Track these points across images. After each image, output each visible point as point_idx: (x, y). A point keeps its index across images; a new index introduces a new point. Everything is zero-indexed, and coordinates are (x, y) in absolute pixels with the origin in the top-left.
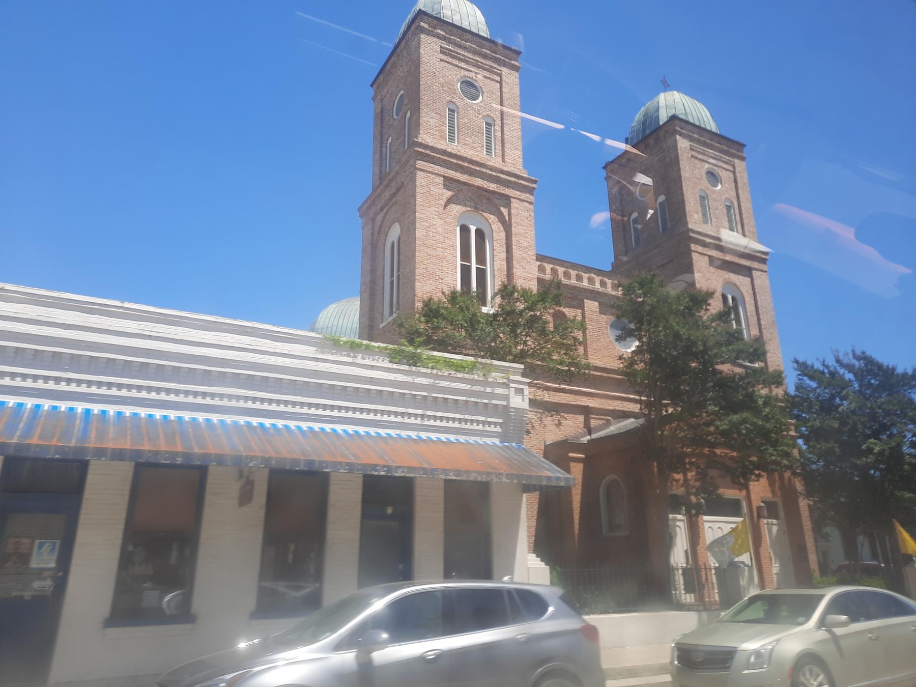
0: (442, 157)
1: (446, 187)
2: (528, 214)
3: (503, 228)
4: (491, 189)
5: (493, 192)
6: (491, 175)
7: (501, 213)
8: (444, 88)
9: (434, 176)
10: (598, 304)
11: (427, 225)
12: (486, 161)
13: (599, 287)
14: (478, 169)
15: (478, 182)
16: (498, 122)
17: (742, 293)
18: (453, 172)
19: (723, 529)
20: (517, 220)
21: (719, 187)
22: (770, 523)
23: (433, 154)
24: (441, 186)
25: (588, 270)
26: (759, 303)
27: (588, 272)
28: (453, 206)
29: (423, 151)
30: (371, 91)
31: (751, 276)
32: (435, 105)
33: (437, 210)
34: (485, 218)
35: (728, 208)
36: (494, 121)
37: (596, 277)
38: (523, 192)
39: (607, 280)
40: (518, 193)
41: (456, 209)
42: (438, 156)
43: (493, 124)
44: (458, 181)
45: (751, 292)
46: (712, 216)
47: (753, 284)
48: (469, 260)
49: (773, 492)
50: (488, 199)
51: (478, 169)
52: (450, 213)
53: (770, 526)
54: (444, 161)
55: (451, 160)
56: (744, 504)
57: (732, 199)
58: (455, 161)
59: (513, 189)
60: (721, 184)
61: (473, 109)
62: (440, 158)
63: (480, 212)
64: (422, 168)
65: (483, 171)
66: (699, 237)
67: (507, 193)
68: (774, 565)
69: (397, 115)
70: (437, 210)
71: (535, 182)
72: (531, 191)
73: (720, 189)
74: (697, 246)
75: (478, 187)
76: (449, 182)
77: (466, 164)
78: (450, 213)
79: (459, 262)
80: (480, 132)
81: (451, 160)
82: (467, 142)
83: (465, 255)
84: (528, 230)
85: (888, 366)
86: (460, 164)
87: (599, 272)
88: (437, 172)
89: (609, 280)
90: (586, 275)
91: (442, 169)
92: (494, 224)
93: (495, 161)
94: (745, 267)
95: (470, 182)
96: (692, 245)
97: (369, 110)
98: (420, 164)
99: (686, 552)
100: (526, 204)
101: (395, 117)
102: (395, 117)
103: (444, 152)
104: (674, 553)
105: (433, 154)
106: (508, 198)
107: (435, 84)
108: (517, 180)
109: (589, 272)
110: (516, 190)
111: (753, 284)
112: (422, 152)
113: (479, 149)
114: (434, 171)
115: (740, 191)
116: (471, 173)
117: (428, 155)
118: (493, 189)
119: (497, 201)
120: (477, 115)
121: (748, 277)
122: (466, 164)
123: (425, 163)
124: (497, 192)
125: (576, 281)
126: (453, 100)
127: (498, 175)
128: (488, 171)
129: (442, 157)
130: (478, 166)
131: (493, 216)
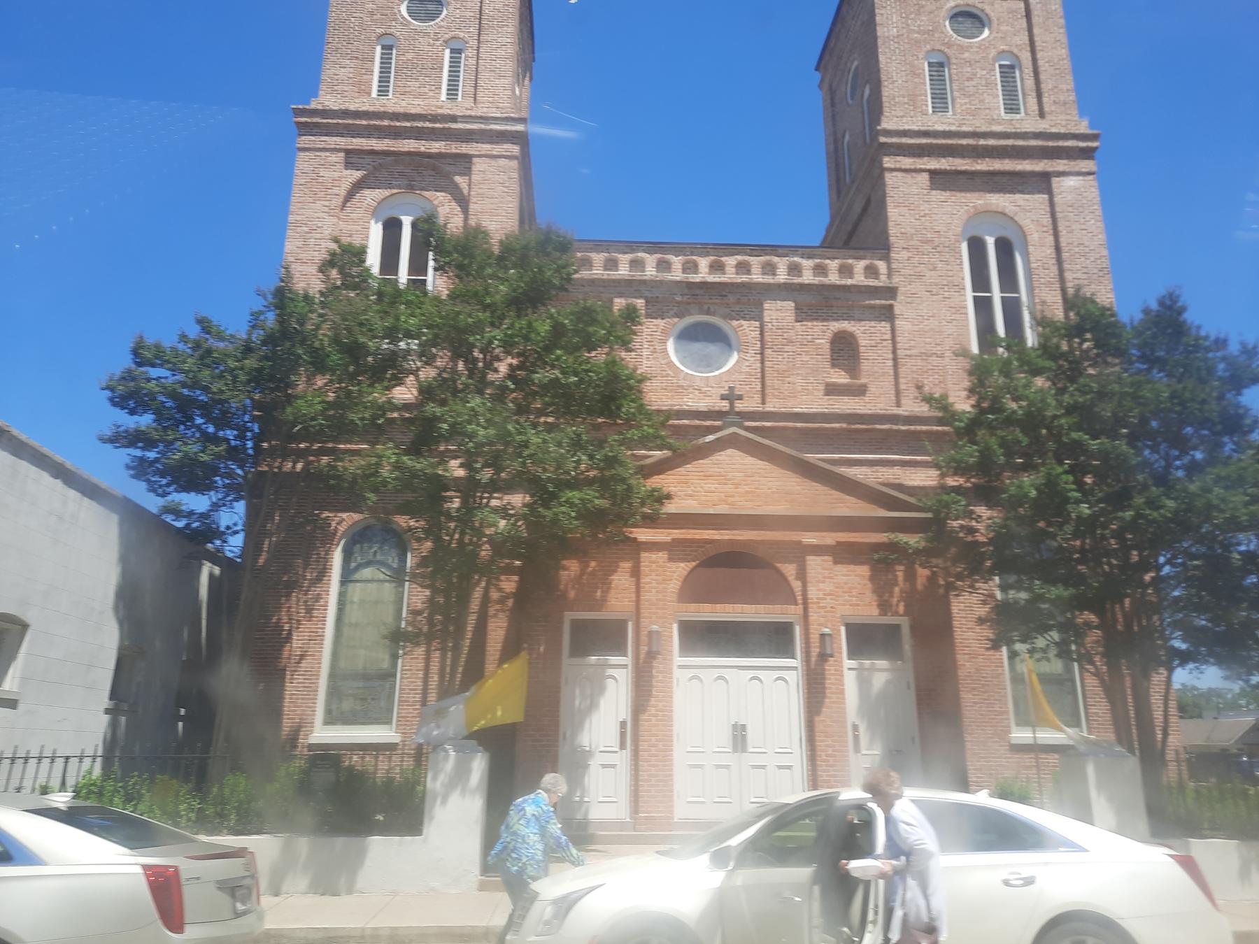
0: (340, 121)
1: (348, 165)
2: (505, 177)
3: (459, 209)
4: (432, 151)
5: (441, 156)
6: (433, 128)
7: (456, 186)
8: (375, 17)
9: (328, 154)
10: (793, 304)
11: (306, 229)
12: (433, 109)
13: (863, 279)
14: (408, 124)
15: (409, 145)
16: (1026, 56)
17: (1020, 227)
18: (363, 140)
19: (764, 682)
20: (480, 191)
21: (986, 33)
22: (867, 666)
23: (325, 121)
24: (341, 167)
25: (630, 246)
26: (1063, 242)
27: (633, 251)
28: (367, 192)
29: (308, 120)
30: (818, 75)
31: (1049, 191)
32: (350, 46)
33: (327, 203)
34: (1009, 216)
35: (1008, 72)
36: (1017, 57)
37: (648, 255)
38: (497, 143)
39: (674, 257)
40: (488, 146)
41: (371, 196)
42: (335, 121)
43: (946, 64)
44: (373, 152)
45: (1047, 220)
46: (956, 94)
47: (1052, 204)
48: (987, 288)
49: (884, 607)
50: (434, 169)
51: (408, 124)
52: (359, 205)
53: (866, 673)
54: (347, 126)
55: (358, 122)
56: (798, 630)
57: (1015, 51)
58: (364, 122)
59: (477, 143)
60: (990, 29)
61: (427, 34)
62: (338, 124)
63: (418, 192)
64: (306, 146)
65: (417, 127)
66: (1061, 143)
67: (465, 152)
68: (864, 752)
69: (852, 99)
70: (327, 203)
71: (1094, 137)
72: (1087, 154)
73: (988, 37)
74: (899, 158)
75: (409, 154)
76: (352, 158)
77: (386, 123)
78: (359, 205)
79: (969, 294)
80: (435, 66)
81: (358, 122)
82: (408, 89)
83: (981, 281)
84: (501, 202)
85: (1146, 311)
86: (375, 125)
87: (807, 252)
88: (332, 146)
89: (676, 256)
90: (626, 256)
91: (343, 139)
92: (443, 205)
93: (1026, 121)
94: (1033, 174)
95: (392, 149)
96: (886, 159)
97: (817, 100)
98: (888, 162)
99: (623, 724)
100: (502, 162)
101: (850, 102)
102: (850, 102)
103: (346, 113)
104: (591, 721)
105: (325, 121)
106: (467, 158)
107: (355, 15)
108: (483, 126)
109: (634, 249)
110: (483, 143)
111: (1052, 204)
112: (306, 122)
113: (431, 94)
114: (328, 146)
115: (1036, 31)
116: (397, 134)
117: (317, 125)
118: (437, 151)
119: (448, 168)
120: (432, 42)
121: (1040, 192)
122: (386, 123)
123: (312, 138)
124: (951, 170)
125: (789, 275)
126: (389, 31)
127: (446, 126)
128: (428, 125)
129: (340, 121)
130: (408, 121)
131: (443, 194)
